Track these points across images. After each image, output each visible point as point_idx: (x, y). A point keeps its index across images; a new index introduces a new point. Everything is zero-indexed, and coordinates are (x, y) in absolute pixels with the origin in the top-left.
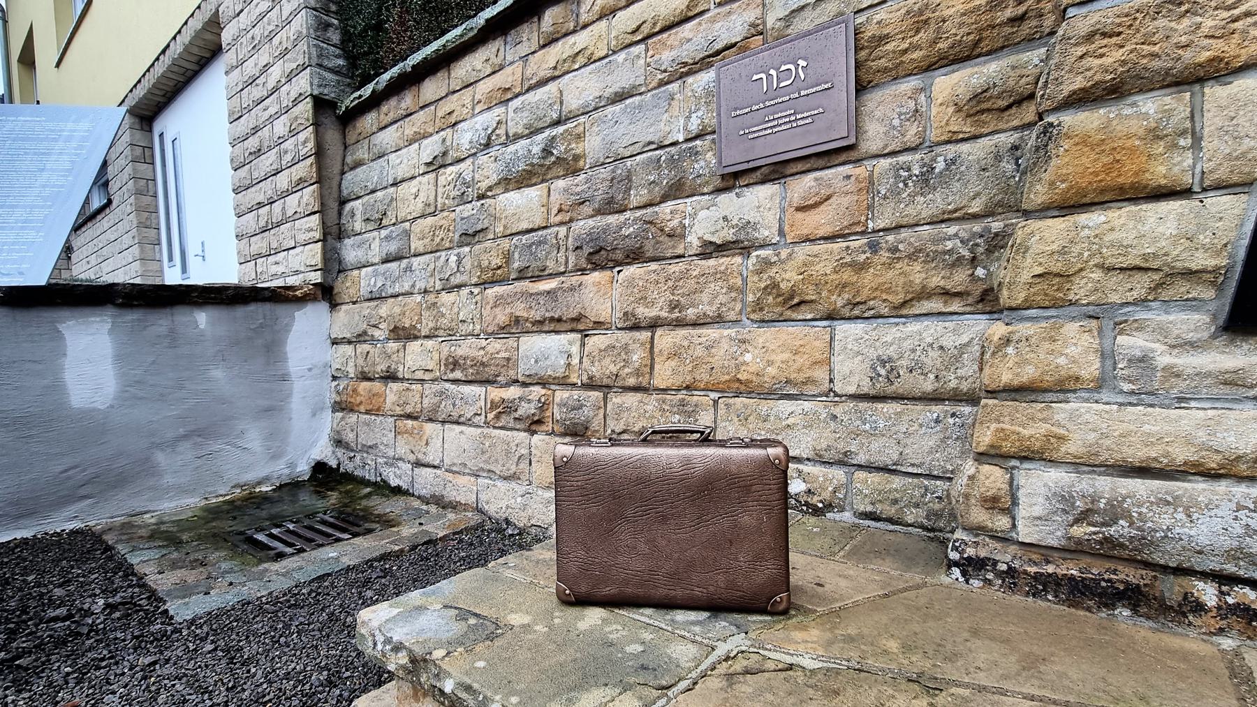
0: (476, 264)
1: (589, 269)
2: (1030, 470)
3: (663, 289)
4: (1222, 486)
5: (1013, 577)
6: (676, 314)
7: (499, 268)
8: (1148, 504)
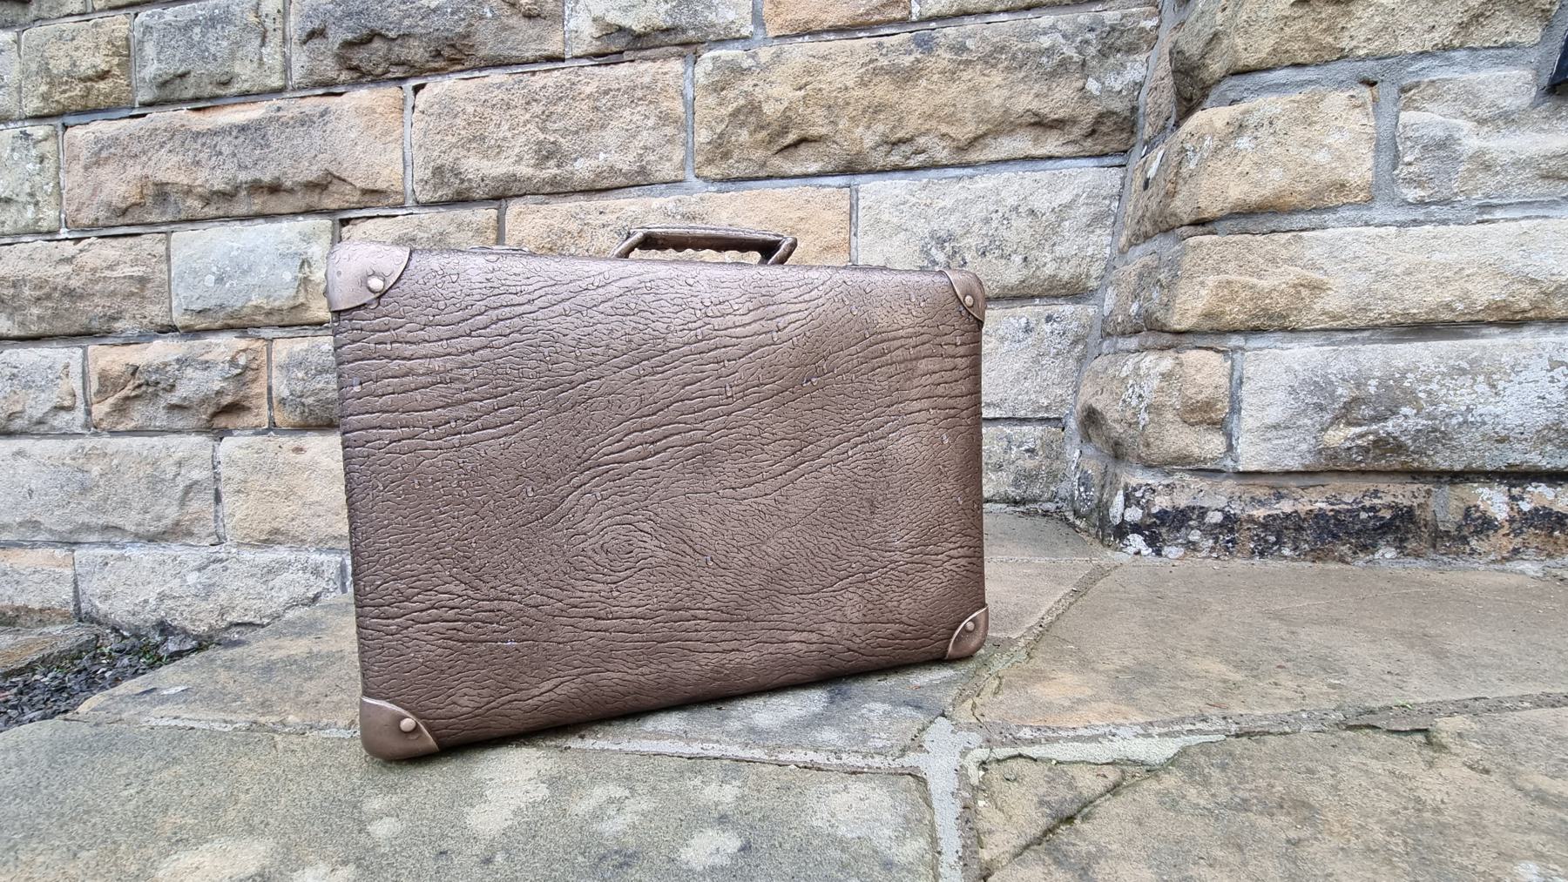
0: (34, 67)
1: (343, 83)
2: (1261, 349)
3: (522, 119)
4: (1527, 337)
5: (1231, 531)
6: (551, 170)
7: (103, 76)
8: (1439, 377)
